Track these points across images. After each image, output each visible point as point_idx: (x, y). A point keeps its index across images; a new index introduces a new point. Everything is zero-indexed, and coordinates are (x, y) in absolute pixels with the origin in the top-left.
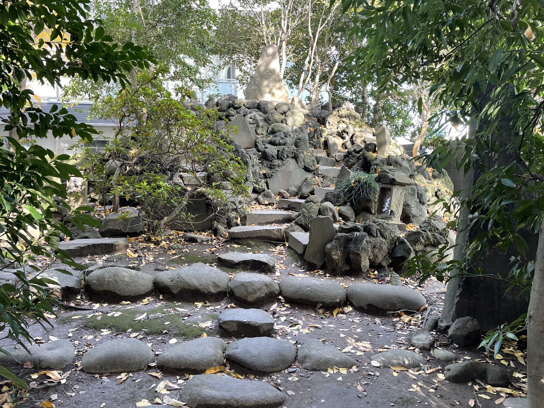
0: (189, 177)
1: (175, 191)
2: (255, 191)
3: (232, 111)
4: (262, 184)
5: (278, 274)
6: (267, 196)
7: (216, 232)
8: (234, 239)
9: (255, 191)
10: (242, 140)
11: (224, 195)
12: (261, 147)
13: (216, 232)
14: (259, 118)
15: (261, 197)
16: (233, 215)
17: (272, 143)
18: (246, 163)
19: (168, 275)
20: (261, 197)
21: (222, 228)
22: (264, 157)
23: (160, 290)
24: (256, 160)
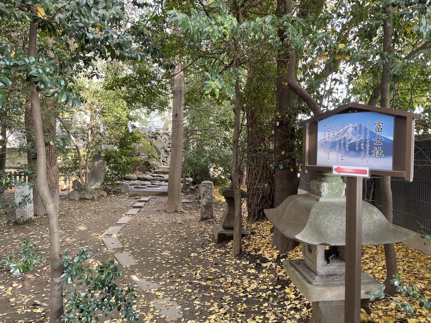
0: (143, 157)
1: (194, 297)
2: (163, 161)
3: (157, 135)
4: (165, 159)
5: (34, 90)
6: (166, 163)
7: (151, 171)
8: (155, 173)
9: (163, 161)
10: (159, 146)
11: (153, 162)
12: (165, 148)
13: (151, 171)
14: (166, 138)
15: (164, 163)
16: (155, 167)
17: (169, 147)
18: (160, 153)
19: (140, 176)
20: (164, 163)
21: (152, 170)
22: (166, 151)
23: (139, 179)
24: (163, 152)
